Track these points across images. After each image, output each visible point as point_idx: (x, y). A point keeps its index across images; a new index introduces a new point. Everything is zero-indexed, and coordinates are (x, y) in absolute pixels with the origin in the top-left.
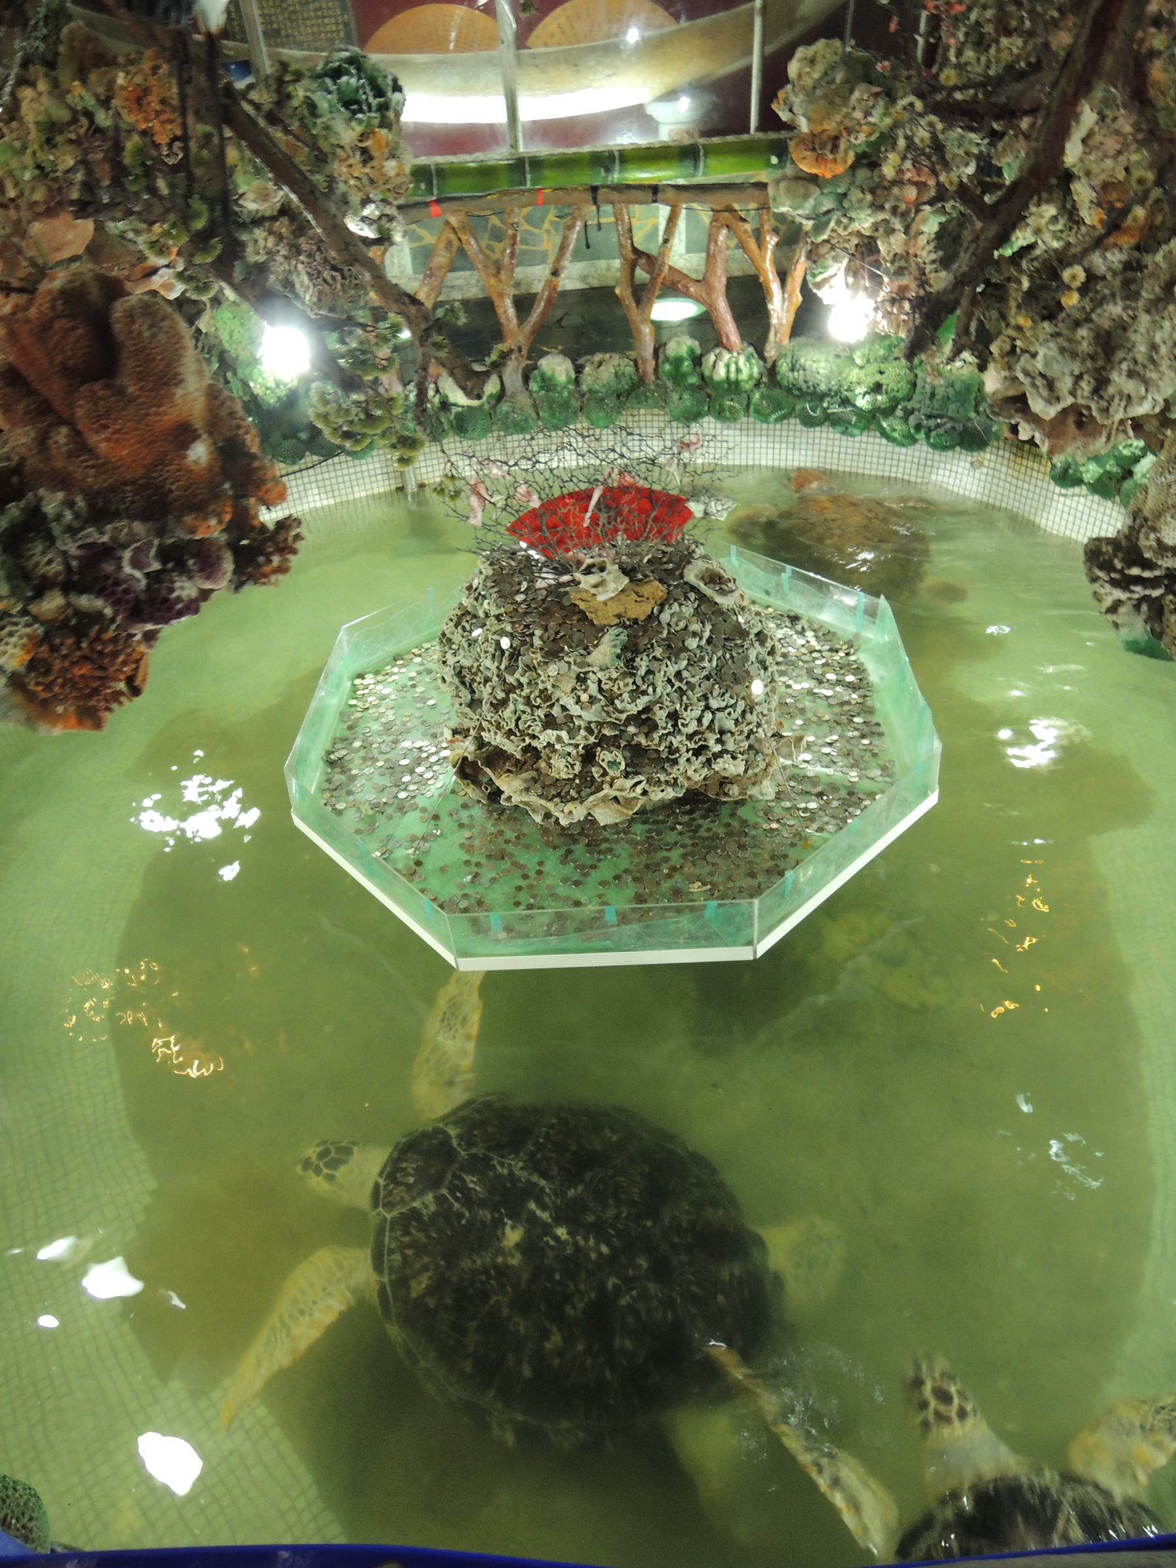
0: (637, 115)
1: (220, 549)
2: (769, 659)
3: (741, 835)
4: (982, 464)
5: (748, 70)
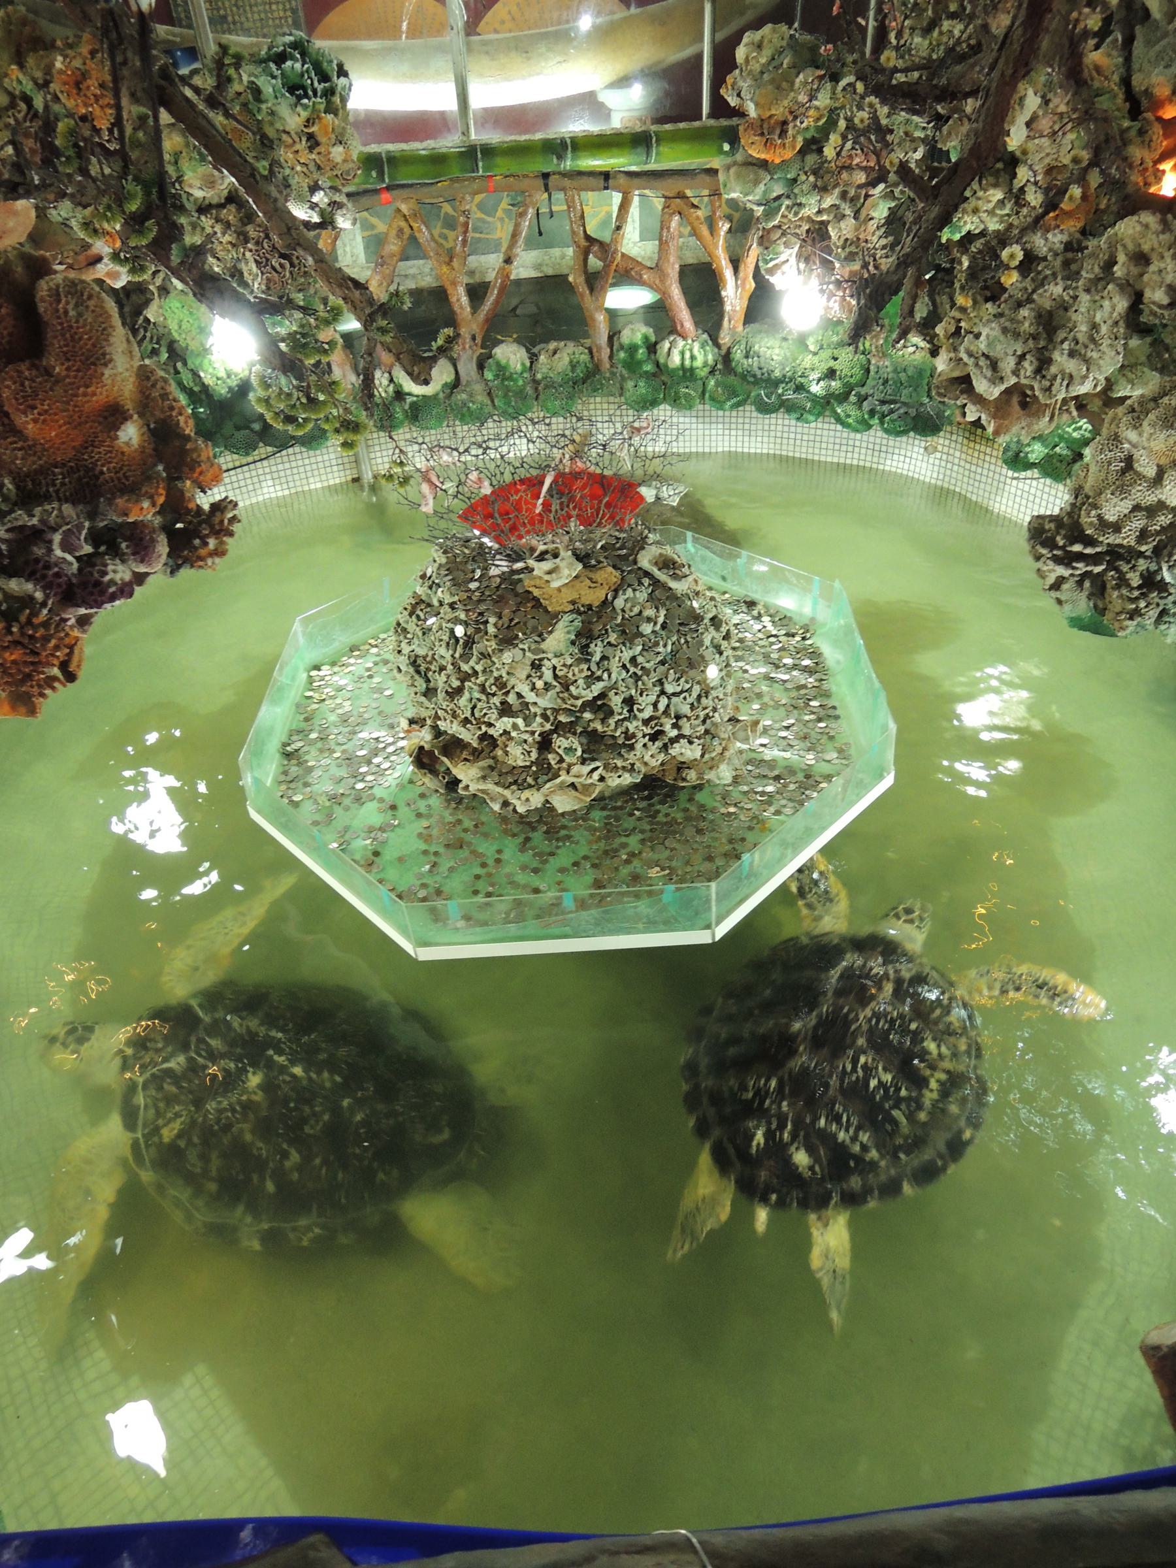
0: (589, 102)
1: (154, 531)
2: (724, 644)
3: (699, 820)
4: (935, 450)
5: (699, 57)
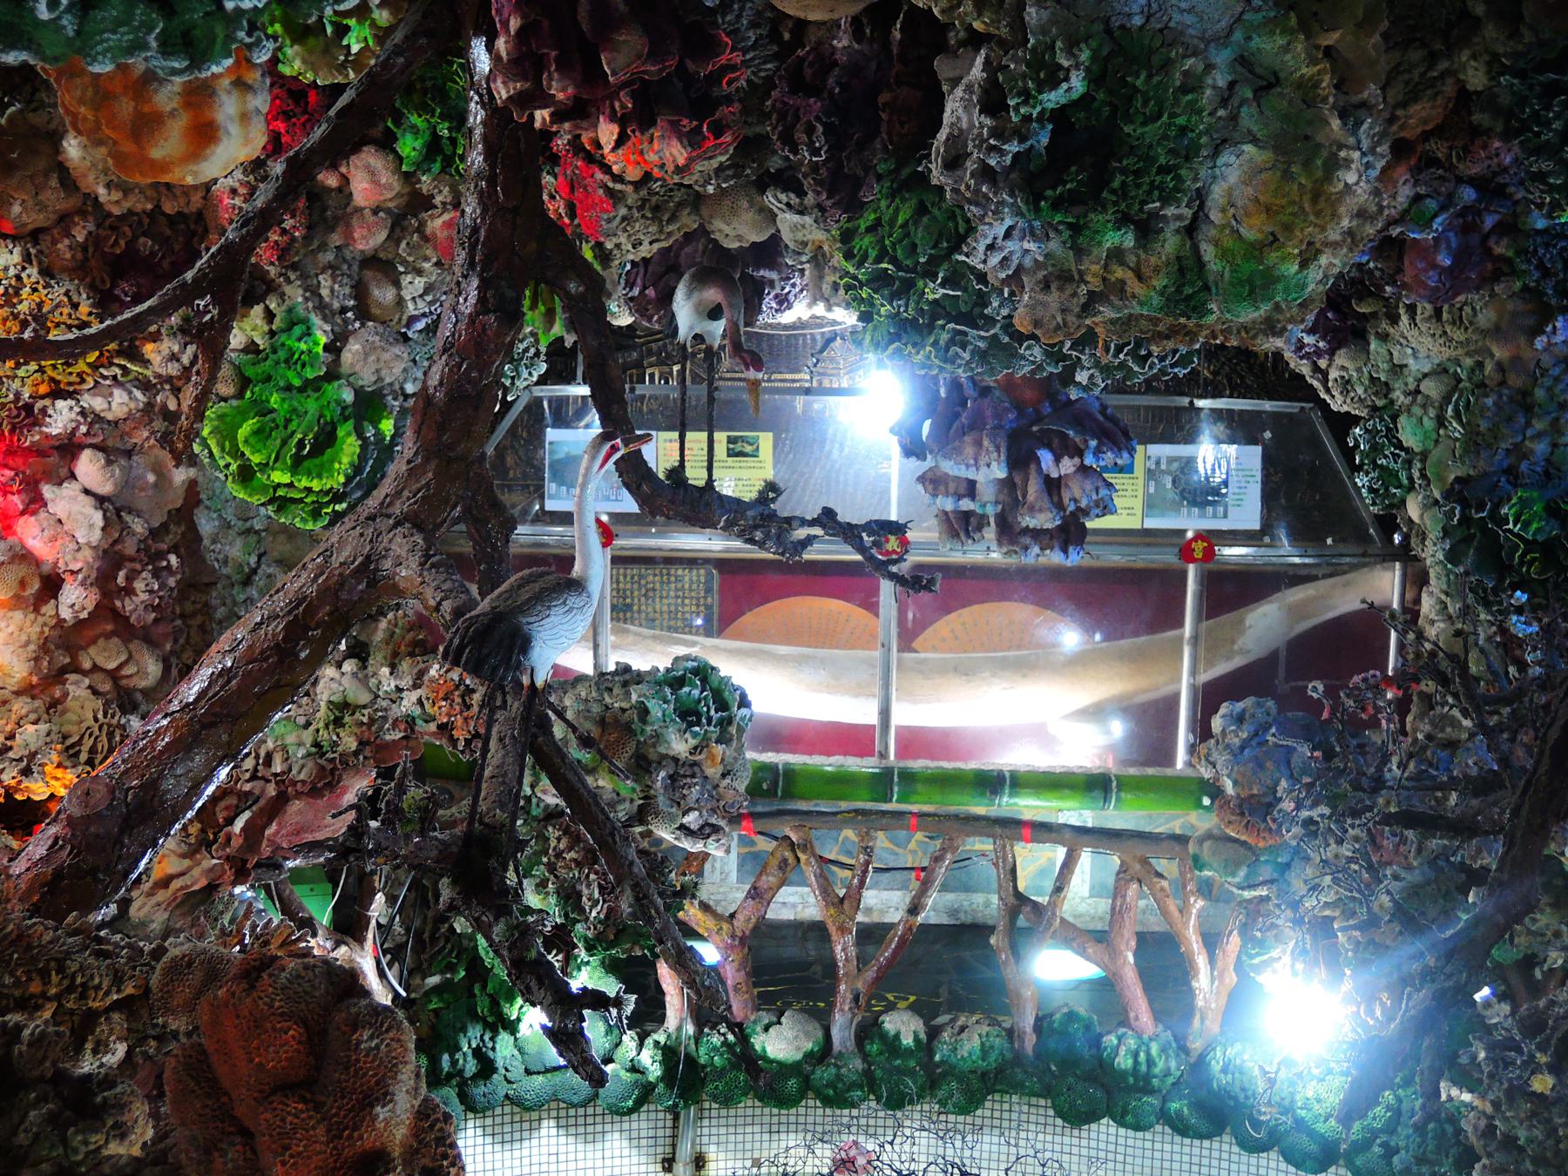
0: (1039, 734)
5: (1174, 700)
